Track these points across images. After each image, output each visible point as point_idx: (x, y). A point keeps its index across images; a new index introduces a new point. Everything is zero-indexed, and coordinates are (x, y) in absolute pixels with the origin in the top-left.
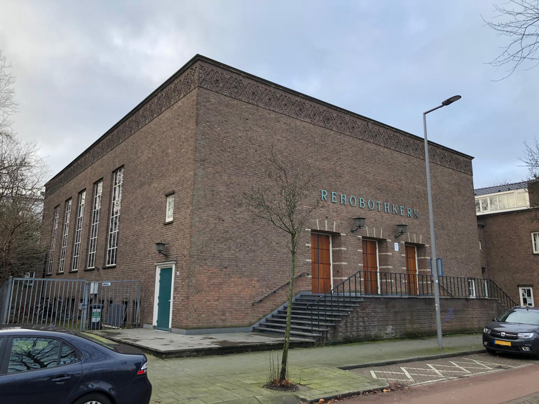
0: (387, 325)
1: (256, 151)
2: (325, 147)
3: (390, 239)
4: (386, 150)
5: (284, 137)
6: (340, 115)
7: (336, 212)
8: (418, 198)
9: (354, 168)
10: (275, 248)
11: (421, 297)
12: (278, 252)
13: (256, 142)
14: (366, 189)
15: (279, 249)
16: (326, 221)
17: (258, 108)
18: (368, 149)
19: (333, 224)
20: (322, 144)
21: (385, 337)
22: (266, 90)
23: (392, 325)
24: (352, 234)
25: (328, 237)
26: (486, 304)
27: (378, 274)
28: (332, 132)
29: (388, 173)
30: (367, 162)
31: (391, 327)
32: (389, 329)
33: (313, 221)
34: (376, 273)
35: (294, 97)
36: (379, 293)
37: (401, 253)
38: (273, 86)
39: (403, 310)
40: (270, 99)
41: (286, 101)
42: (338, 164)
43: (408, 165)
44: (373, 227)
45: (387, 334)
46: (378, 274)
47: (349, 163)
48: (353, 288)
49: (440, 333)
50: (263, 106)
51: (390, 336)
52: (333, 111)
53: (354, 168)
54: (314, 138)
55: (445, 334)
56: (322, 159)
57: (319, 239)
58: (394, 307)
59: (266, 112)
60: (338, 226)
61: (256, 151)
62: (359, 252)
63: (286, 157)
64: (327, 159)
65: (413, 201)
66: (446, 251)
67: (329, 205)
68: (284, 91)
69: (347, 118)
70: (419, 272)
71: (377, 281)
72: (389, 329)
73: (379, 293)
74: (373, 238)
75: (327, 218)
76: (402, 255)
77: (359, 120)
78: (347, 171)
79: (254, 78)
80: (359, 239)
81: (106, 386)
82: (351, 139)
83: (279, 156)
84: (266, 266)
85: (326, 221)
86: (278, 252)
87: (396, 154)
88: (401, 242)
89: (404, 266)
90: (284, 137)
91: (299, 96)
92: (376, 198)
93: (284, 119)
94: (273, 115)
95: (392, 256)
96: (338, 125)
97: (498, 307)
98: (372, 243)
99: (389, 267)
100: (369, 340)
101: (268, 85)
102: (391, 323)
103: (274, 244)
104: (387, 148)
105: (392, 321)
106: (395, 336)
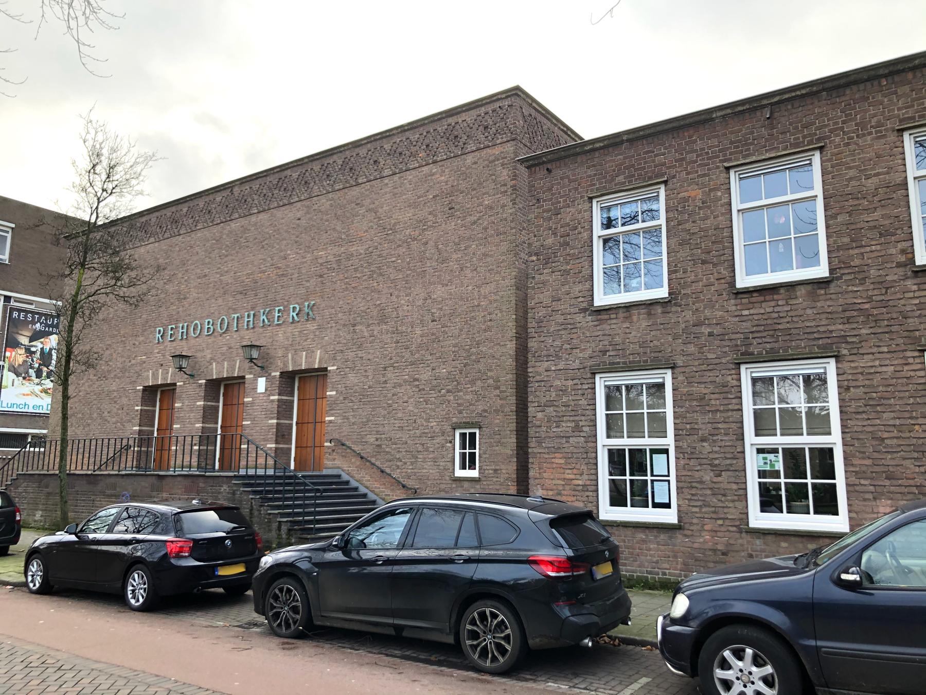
0: (37, 510)
3: (251, 373)
8: (321, 276)
15: (109, 419)
26: (201, 485)
27: (219, 437)
29: (260, 256)
32: (38, 515)
33: (146, 374)
36: (217, 467)
37: (269, 395)
44: (224, 360)
45: (35, 521)
46: (219, 437)
48: (251, 463)
58: (47, 487)
62: (198, 406)
65: (308, 288)
66: (385, 369)
72: (38, 515)
73: (217, 467)
76: (272, 398)
77: (314, 163)
80: (200, 385)
81: (776, 618)
87: (279, 213)
88: (273, 374)
89: (272, 418)
95: (252, 403)
97: (234, 493)
98: (225, 389)
102: (41, 506)
104: (264, 211)
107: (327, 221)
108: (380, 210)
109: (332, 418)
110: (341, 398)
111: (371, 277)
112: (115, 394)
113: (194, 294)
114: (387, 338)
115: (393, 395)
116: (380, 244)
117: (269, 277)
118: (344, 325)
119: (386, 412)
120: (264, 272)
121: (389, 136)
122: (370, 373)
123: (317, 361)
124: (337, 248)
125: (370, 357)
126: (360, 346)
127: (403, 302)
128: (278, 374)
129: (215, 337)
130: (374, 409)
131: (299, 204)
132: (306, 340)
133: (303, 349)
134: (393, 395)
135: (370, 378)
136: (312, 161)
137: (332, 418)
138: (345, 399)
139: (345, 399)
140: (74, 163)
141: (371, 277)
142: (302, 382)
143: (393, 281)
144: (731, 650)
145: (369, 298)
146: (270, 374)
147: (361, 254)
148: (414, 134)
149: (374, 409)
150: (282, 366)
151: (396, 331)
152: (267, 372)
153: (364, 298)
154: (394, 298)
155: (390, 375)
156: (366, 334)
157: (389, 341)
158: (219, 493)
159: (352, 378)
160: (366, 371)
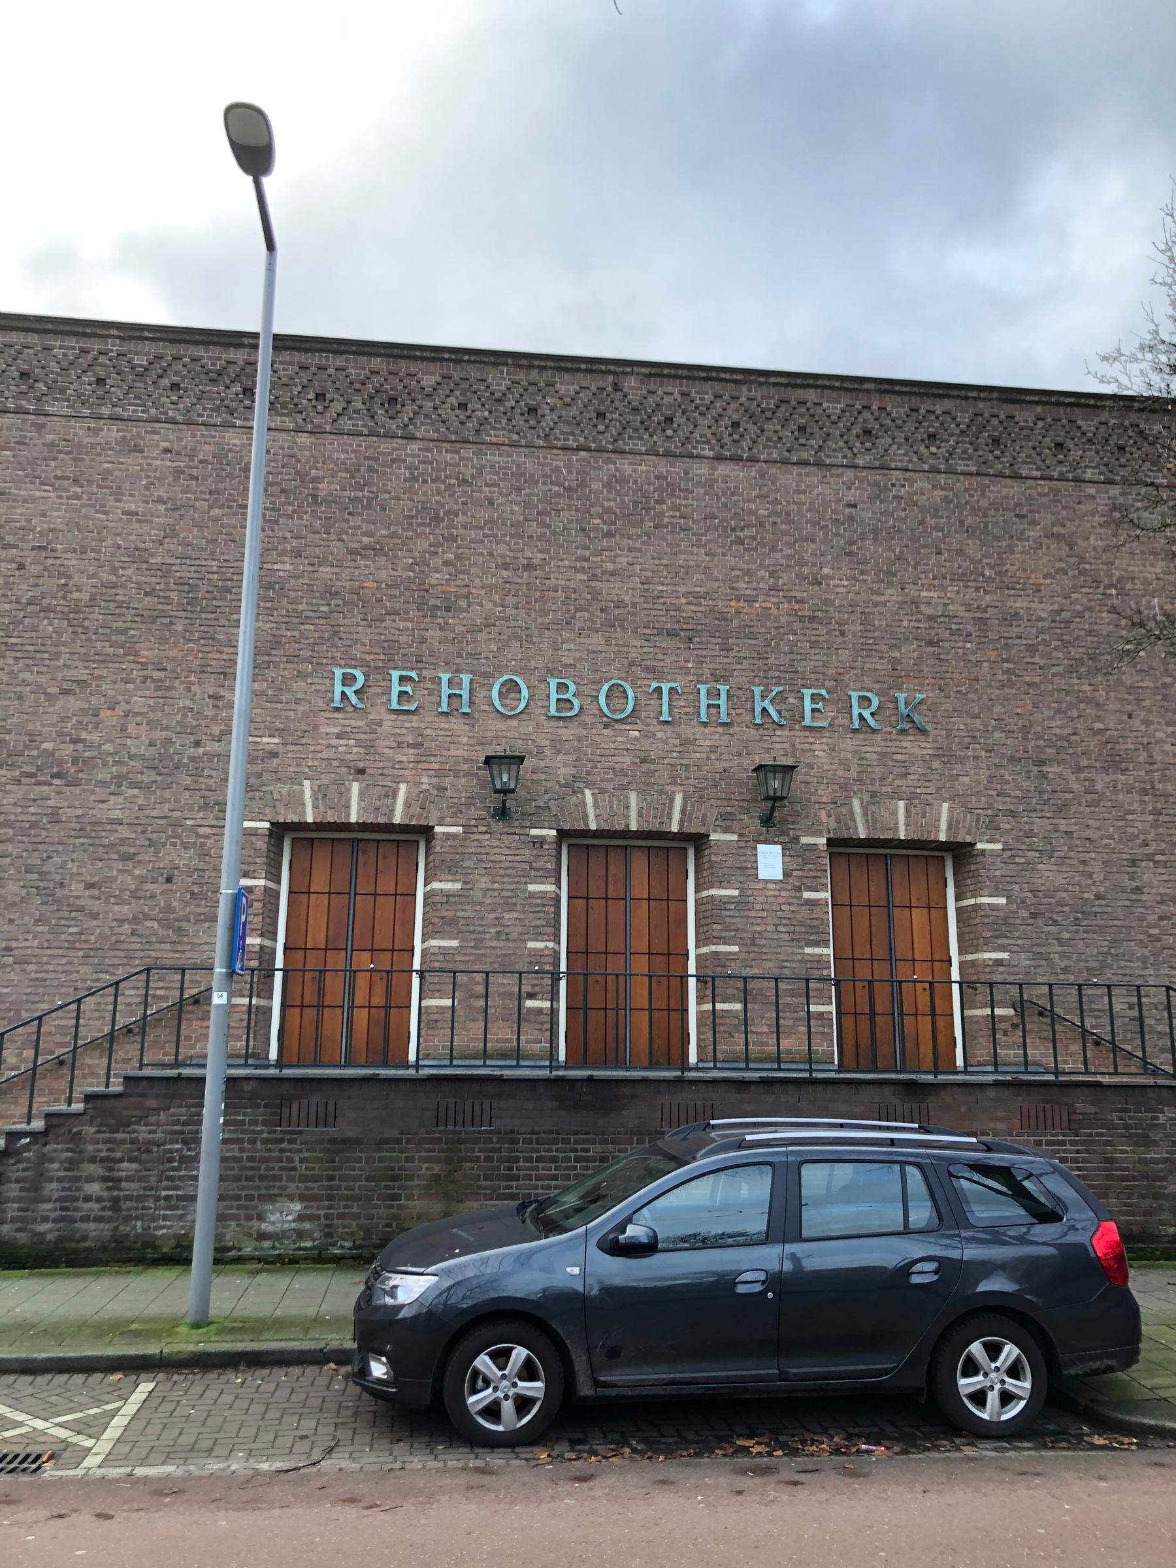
1: (21, 567)
2: (369, 506)
4: (723, 469)
5: (160, 501)
6: (456, 376)
7: (415, 746)
8: (931, 643)
9: (530, 567)
10: (81, 902)
11: (287, 1072)
12: (94, 916)
13: (23, 540)
14: (596, 641)
15: (96, 906)
16: (355, 786)
17: (41, 420)
18: (617, 482)
19: (395, 794)
20: (355, 500)
21: (248, 1250)
22: (303, 367)
23: (302, 1198)
24: (498, 826)
25: (942, 858)
27: (692, 982)
28: (414, 447)
29: (730, 561)
30: (609, 535)
31: (297, 1207)
34: (684, 978)
35: (216, 352)
36: (960, 1062)
37: (799, 889)
38: (115, 332)
39: (391, 1133)
40: (100, 382)
41: (177, 374)
42: (437, 562)
43: (866, 514)
44: (625, 787)
45: (262, 1236)
46: (279, 976)
47: (502, 549)
49: (201, 1252)
50: (66, 411)
51: (286, 1248)
52: (415, 367)
53: (530, 567)
54: (315, 480)
55: (224, 1258)
56: (352, 552)
57: (872, 874)
59: (78, 430)
60: (421, 799)
61: (21, 567)
63: (164, 570)
64: (377, 550)
65: (895, 662)
66: (1134, 862)
67: (380, 723)
68: (172, 341)
69: (499, 380)
70: (962, 965)
71: (284, 1005)
73: (960, 1062)
74: (626, 834)
75: (362, 771)
78: (488, 580)
79: (304, 345)
80: (539, 842)
82: (519, 456)
83: (129, 572)
84: (31, 967)
85: (355, 786)
86: (94, 916)
87: (789, 478)
90: (160, 501)
91: (242, 346)
92: (651, 670)
93: (166, 436)
94: (112, 433)
96: (451, 416)
99: (722, 948)
100: (126, 1262)
101: (93, 335)
103: (76, 888)
104: (735, 459)
105: (304, 1179)
106: (321, 1249)
107: (937, 528)
108: (1081, 543)
109: (1005, 955)
110: (1024, 913)
111: (1070, 671)
112: (124, 832)
113: (484, 606)
114: (1132, 801)
115: (1161, 918)
116: (1091, 609)
117: (765, 613)
118: (1012, 759)
119: (1146, 952)
120: (750, 600)
121: (1095, 406)
122: (1095, 867)
123: (944, 825)
124: (971, 594)
125: (1089, 833)
126: (1061, 810)
127: (1159, 735)
128: (824, 841)
129: (584, 726)
130: (1115, 943)
131: (849, 474)
132: (904, 776)
133: (897, 795)
134: (1161, 918)
135: (1098, 877)
136: (559, 369)
137: (1005, 955)
138: (1034, 916)
139: (1034, 916)
140: (252, 144)
141: (1070, 671)
142: (882, 869)
143: (1131, 690)
144: (1018, 1359)
145: (1075, 713)
146: (796, 840)
147: (1041, 619)
148: (1026, 414)
149: (1115, 943)
150: (832, 824)
151: (1149, 790)
152: (784, 833)
153: (1059, 711)
154: (1136, 723)
155: (1147, 875)
156: (1075, 786)
157: (1135, 806)
158: (1152, 1126)
159: (1048, 874)
160: (1084, 862)
